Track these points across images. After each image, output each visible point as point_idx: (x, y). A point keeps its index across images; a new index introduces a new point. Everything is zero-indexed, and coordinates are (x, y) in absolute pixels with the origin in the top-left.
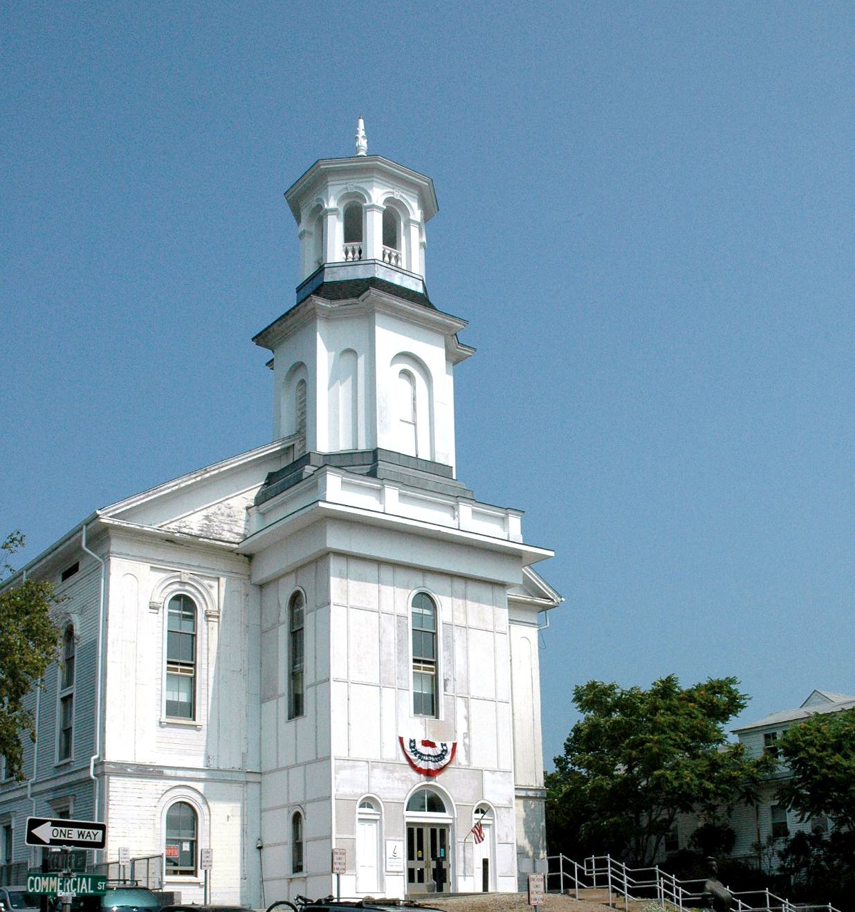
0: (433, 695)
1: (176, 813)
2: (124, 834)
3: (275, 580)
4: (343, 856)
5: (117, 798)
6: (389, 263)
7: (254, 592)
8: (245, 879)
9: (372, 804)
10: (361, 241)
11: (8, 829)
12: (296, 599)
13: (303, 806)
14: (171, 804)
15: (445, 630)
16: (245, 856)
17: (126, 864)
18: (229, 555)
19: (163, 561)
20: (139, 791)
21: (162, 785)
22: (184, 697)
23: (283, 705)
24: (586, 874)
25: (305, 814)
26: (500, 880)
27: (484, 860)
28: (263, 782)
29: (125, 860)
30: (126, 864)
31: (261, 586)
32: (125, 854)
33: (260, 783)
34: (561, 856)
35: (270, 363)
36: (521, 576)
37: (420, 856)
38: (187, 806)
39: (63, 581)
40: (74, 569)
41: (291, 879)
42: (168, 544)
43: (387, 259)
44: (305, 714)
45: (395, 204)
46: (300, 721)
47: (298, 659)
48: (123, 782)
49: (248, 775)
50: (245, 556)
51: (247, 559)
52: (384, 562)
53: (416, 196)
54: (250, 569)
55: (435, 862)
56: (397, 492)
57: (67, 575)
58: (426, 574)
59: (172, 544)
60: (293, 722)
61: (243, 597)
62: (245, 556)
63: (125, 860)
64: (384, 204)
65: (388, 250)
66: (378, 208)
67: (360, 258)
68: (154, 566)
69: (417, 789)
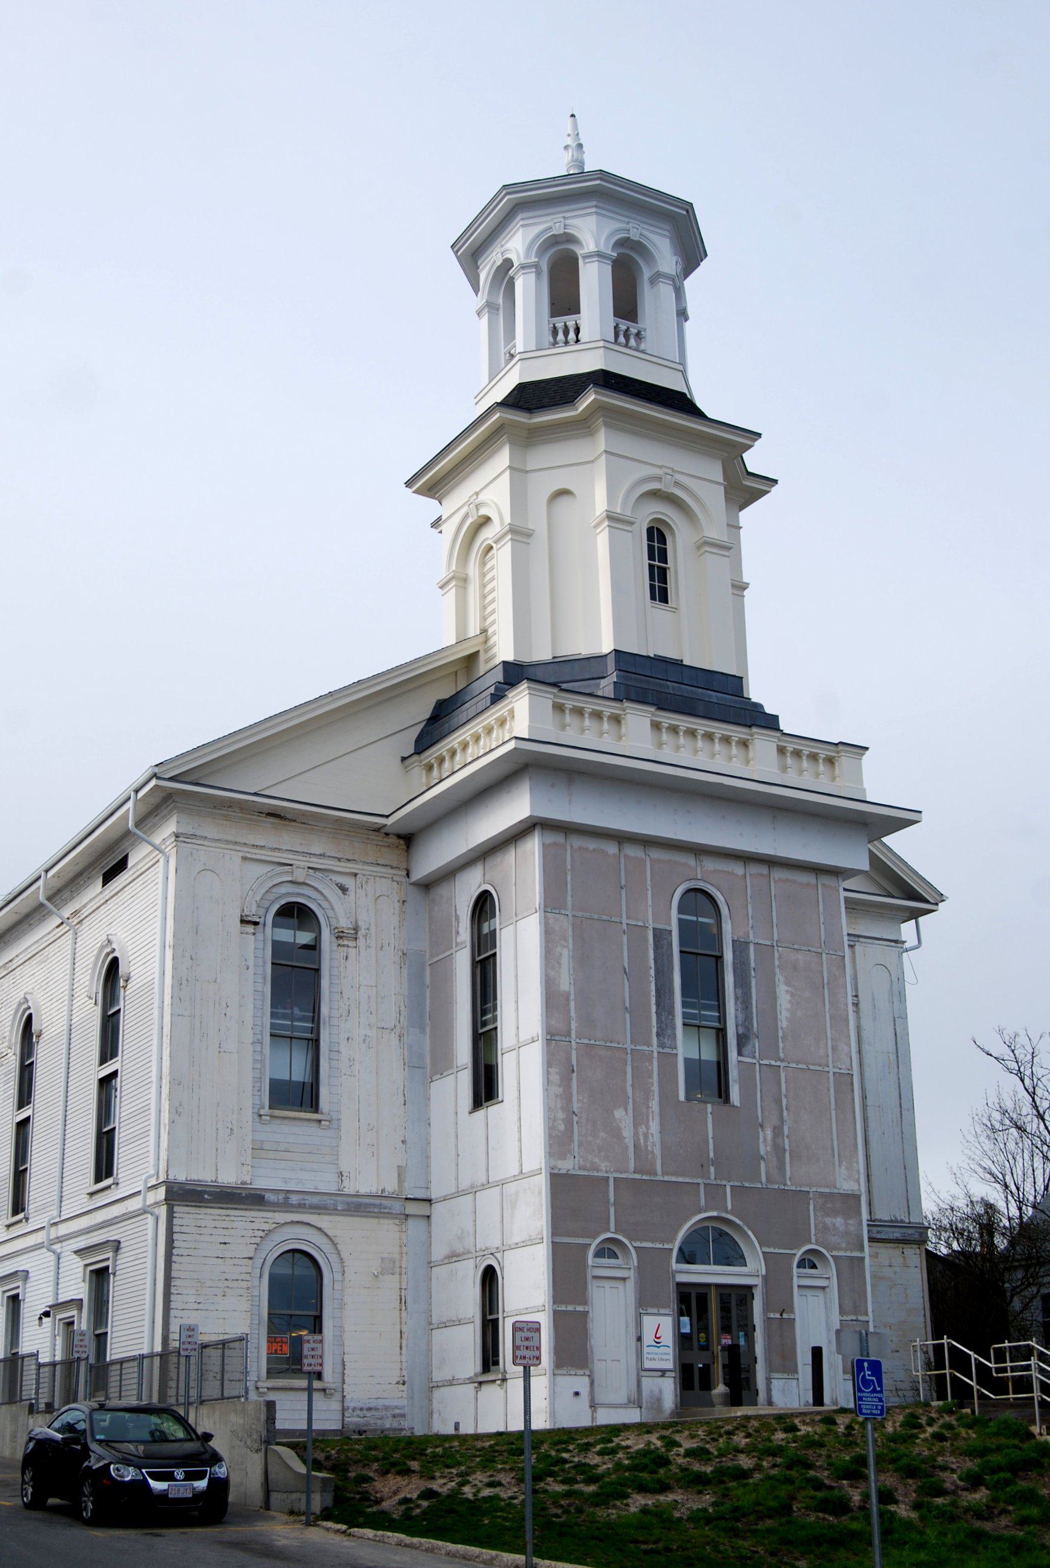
0: (718, 1063)
1: (285, 1270)
2: (196, 1306)
3: (450, 873)
4: (319, 1346)
5: (186, 1245)
6: (626, 346)
7: (414, 894)
8: (404, 1383)
9: (617, 1251)
10: (579, 312)
11: (15, 1301)
12: (484, 905)
13: (498, 1255)
14: (276, 1255)
15: (737, 953)
16: (404, 1345)
17: (192, 1353)
18: (373, 835)
19: (263, 847)
20: (225, 1232)
21: (262, 1219)
22: (299, 1073)
23: (463, 1082)
24: (995, 1375)
25: (502, 1269)
26: (782, 1382)
27: (813, 1348)
28: (433, 1218)
29: (190, 1347)
30: (192, 1353)
31: (427, 886)
32: (81, 1340)
33: (428, 1217)
34: (945, 1340)
35: (436, 524)
36: (867, 855)
37: (703, 1341)
38: (306, 1260)
39: (103, 886)
40: (121, 866)
41: (480, 1383)
42: (272, 820)
43: (622, 339)
44: (500, 1099)
45: (632, 249)
46: (492, 1111)
47: (490, 1005)
48: (197, 1216)
49: (409, 1204)
50: (399, 836)
51: (402, 842)
52: (823, 870)
53: (667, 234)
54: (408, 861)
55: (840, 1356)
56: (648, 722)
57: (109, 877)
58: (702, 857)
59: (276, 821)
60: (481, 1113)
61: (397, 905)
62: (399, 836)
63: (190, 1347)
64: (613, 250)
65: (624, 325)
66: (666, 276)
67: (577, 341)
68: (249, 855)
69: (692, 1225)
